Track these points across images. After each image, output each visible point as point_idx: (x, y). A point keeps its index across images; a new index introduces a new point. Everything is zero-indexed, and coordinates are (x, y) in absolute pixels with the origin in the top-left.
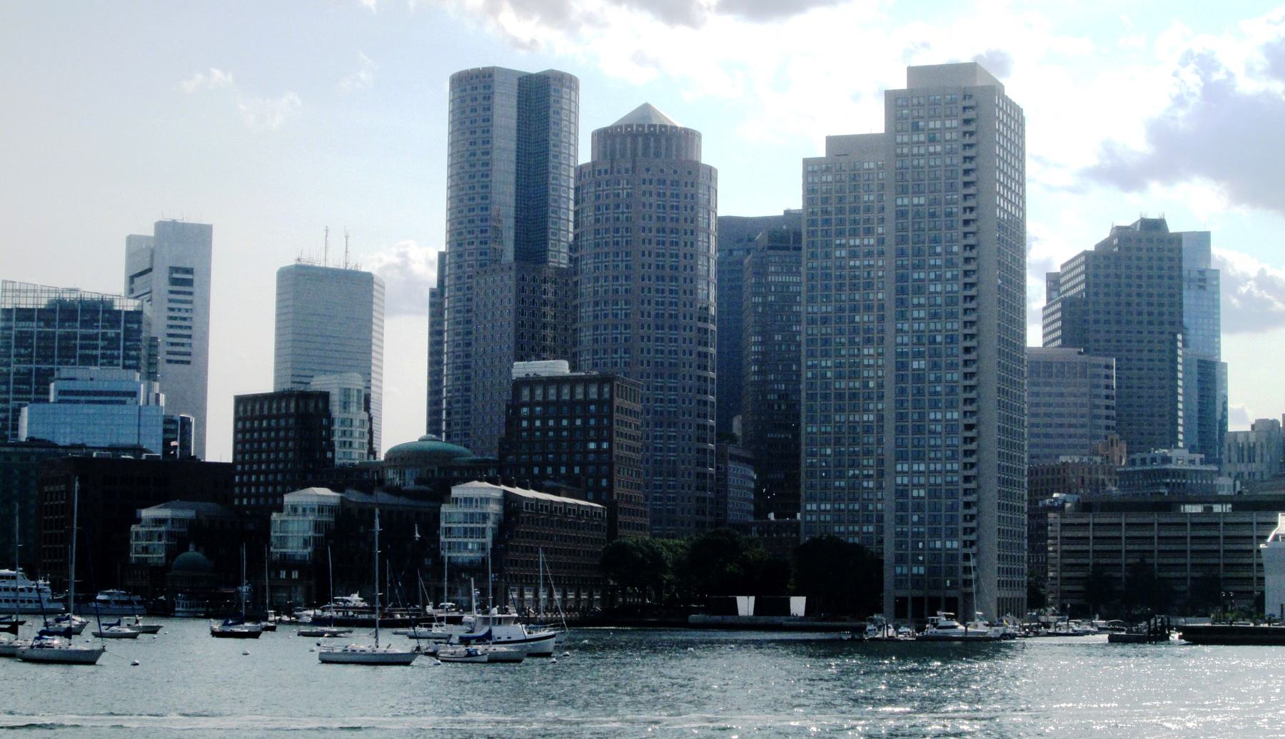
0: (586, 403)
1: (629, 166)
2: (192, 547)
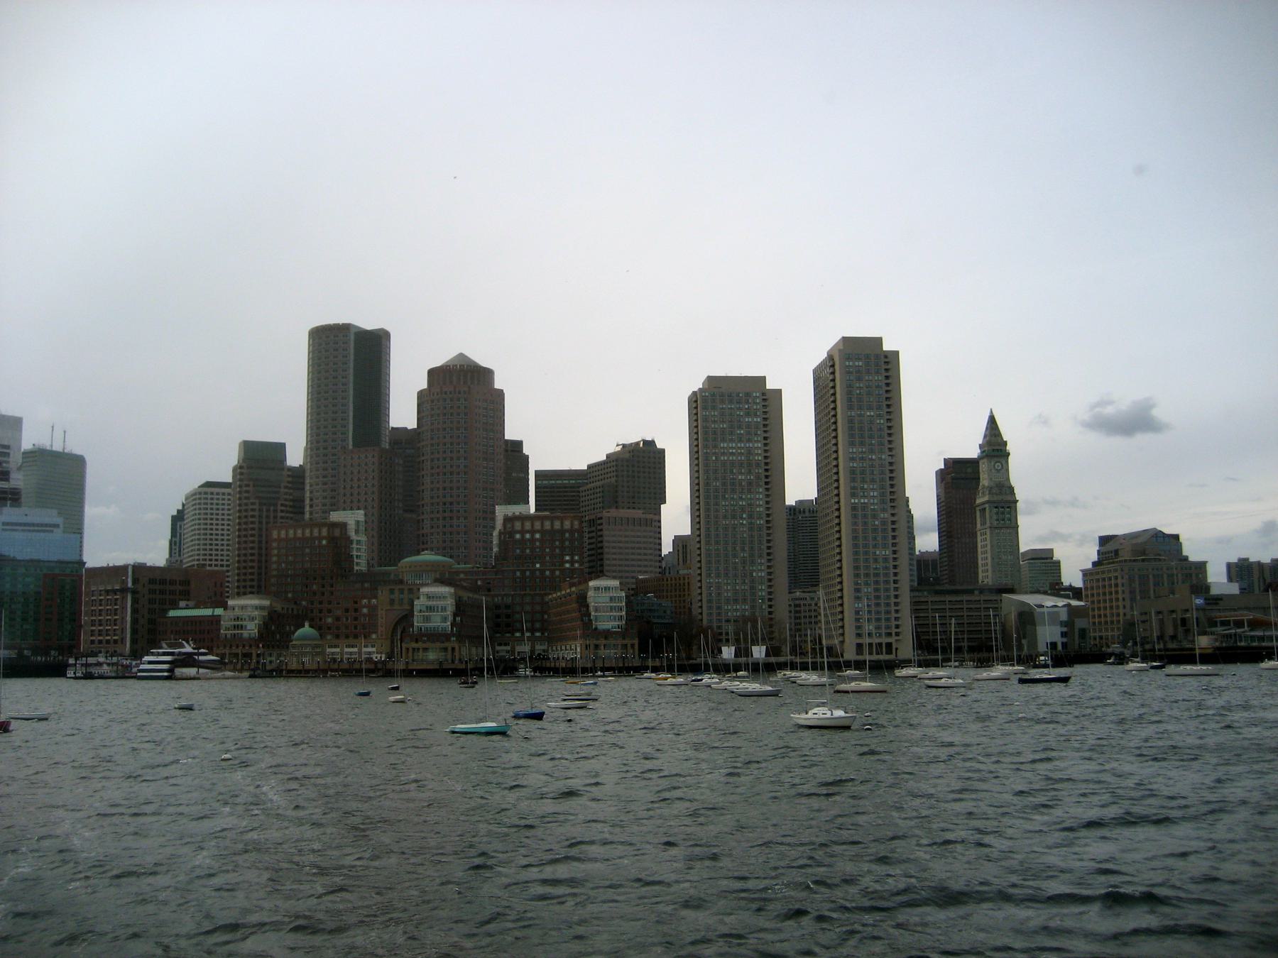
0: (562, 531)
1: (466, 389)
2: (307, 624)
